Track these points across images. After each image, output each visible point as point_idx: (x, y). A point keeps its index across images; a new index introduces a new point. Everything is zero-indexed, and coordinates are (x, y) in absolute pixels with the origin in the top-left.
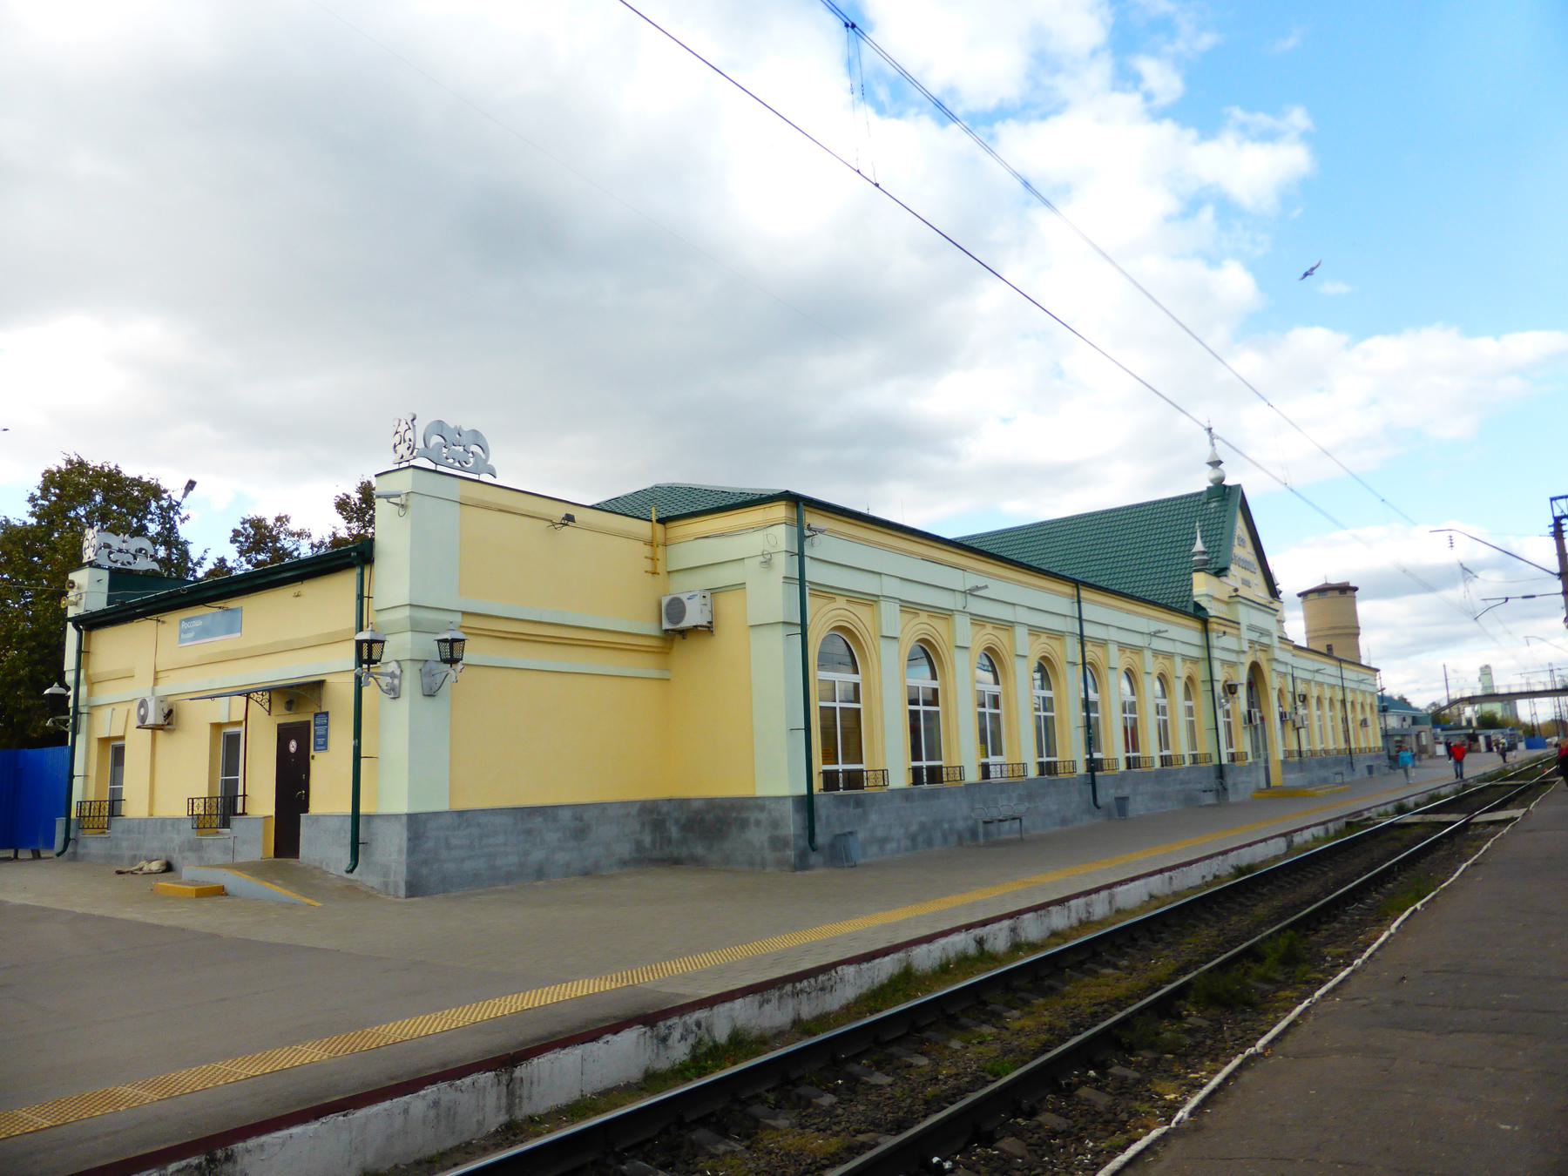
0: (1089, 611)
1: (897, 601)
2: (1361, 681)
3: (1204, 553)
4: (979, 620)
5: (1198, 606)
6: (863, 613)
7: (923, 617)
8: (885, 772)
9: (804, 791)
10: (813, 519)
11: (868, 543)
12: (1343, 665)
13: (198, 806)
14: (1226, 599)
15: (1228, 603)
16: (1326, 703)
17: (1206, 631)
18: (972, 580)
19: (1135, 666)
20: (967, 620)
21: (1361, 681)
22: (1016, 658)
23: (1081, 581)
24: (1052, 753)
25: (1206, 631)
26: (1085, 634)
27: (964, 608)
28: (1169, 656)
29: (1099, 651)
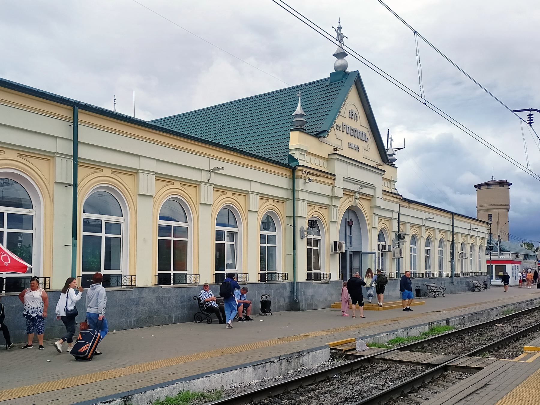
0: (84, 133)
2: (473, 230)
3: (301, 115)
4: (220, 189)
5: (292, 159)
6: (241, 199)
9: (293, 280)
10: (82, 117)
14: (326, 156)
15: (327, 160)
16: (477, 248)
17: (294, 178)
18: (215, 164)
19: (431, 236)
21: (473, 230)
22: (139, 198)
23: (455, 213)
25: (294, 178)
26: (400, 220)
27: (208, 180)
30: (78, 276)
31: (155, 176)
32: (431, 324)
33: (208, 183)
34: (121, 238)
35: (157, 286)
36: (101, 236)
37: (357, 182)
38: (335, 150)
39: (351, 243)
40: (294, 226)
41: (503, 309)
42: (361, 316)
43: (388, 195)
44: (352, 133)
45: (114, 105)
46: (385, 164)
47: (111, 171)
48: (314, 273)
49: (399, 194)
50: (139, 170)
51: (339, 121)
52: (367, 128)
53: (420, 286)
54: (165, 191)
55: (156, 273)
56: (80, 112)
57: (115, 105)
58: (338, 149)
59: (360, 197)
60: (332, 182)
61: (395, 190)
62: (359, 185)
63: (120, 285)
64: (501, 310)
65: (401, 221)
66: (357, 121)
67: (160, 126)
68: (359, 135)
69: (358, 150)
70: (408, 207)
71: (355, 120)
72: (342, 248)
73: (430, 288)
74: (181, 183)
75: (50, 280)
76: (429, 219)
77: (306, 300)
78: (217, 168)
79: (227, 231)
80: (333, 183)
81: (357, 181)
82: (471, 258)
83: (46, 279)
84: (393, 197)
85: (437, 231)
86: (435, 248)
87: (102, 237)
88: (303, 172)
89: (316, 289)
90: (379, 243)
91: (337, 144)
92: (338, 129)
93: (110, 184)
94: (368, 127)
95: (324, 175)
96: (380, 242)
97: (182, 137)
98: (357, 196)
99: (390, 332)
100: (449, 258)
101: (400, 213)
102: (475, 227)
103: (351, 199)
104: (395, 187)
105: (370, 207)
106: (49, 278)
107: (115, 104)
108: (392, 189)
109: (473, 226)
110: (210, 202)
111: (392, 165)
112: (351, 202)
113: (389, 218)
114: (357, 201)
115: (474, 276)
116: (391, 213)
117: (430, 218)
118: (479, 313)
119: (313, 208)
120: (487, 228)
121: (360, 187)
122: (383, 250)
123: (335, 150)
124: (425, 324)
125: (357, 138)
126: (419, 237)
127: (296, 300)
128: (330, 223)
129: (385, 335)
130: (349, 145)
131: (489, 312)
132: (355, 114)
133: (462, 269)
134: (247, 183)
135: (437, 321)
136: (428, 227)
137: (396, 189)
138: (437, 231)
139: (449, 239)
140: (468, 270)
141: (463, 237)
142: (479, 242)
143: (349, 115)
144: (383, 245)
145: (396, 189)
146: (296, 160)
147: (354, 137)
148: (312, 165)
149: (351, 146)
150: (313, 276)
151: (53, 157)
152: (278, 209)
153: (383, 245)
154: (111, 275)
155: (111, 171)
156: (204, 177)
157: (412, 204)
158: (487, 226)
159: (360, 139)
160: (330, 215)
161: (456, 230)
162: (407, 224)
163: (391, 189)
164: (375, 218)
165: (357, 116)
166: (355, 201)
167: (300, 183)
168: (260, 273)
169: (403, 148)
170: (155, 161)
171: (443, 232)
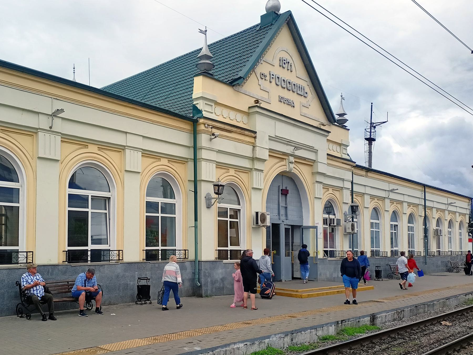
0: (428, 196)
1: (407, 202)
2: (450, 204)
5: (197, 111)
7: (93, 148)
8: (187, 251)
11: (153, 122)
12: (426, 190)
13: (446, 253)
14: (246, 109)
15: (248, 114)
17: (195, 133)
18: (392, 187)
19: (442, 217)
20: (389, 201)
21: (450, 204)
24: (413, 247)
25: (195, 133)
27: (388, 196)
28: (455, 213)
29: (359, 198)
30: (143, 249)
31: (141, 152)
32: (341, 323)
33: (50, 130)
34: (106, 213)
35: (145, 262)
36: (88, 211)
37: (289, 142)
38: (257, 102)
39: (286, 215)
40: (196, 192)
41: (467, 297)
42: (253, 307)
43: (335, 161)
44: (284, 84)
45: (73, 73)
46: (332, 124)
47: (98, 147)
48: (230, 250)
49: (353, 161)
50: (189, 159)
51: (262, 68)
52: (307, 82)
53: (380, 267)
54: (152, 169)
55: (216, 249)
56: (426, 188)
57: (74, 74)
58: (259, 101)
59: (295, 161)
60: (252, 140)
61: (347, 155)
62: (293, 146)
63: (109, 259)
64: (463, 298)
65: (427, 206)
66: (291, 71)
67: (130, 98)
68: (295, 88)
69: (293, 105)
70: (366, 176)
71: (288, 70)
72: (266, 219)
73: (394, 269)
74: (98, 147)
75: (33, 254)
76: (451, 204)
77: (213, 283)
78: (58, 110)
79: (230, 208)
80: (254, 142)
81: (289, 141)
82: (451, 236)
83: (120, 251)
84: (342, 163)
85: (457, 214)
86: (403, 224)
87: (89, 212)
88: (206, 126)
89: (228, 270)
90: (326, 216)
91: (260, 95)
92: (278, 83)
93: (6, 146)
94: (308, 79)
95: (239, 131)
96: (328, 215)
97: (135, 104)
98: (292, 159)
99: (253, 342)
100: (422, 234)
101: (354, 182)
102: (453, 201)
103: (283, 163)
104: (347, 152)
105: (311, 173)
106: (122, 251)
107: (74, 72)
108: (343, 155)
109: (450, 201)
110: (130, 168)
111: (343, 126)
112: (283, 166)
113: (453, 212)
114: (292, 166)
115: (454, 256)
116: (341, 182)
117: (394, 190)
118: (429, 304)
119: (227, 171)
120: (469, 203)
121: (294, 148)
122: (331, 224)
123: (257, 101)
124: (328, 324)
125: (291, 91)
126: (382, 211)
127: (197, 284)
128: (37, 161)
129: (241, 345)
130: (279, 99)
131: (444, 302)
132: (289, 62)
133: (439, 247)
134: (363, 187)
135: (353, 318)
136: (450, 211)
137: (348, 154)
138: (457, 214)
139: (421, 214)
140: (445, 248)
141: (451, 214)
142: (459, 219)
143: (280, 64)
144: (332, 219)
145: (348, 155)
146: (200, 112)
147: (288, 89)
148: (224, 119)
149: (281, 100)
150: (229, 255)
151: (36, 133)
152: (175, 171)
153: (332, 219)
154: (102, 250)
155: (168, 160)
156: (44, 123)
157: (370, 173)
158: (468, 201)
159: (296, 92)
160: (251, 179)
161: (428, 204)
162: (366, 196)
163: (342, 154)
164: (319, 188)
165: (291, 66)
166: (289, 165)
167: (203, 140)
168: (218, 250)
169: (386, 122)
170: (370, 187)
171: (440, 211)
